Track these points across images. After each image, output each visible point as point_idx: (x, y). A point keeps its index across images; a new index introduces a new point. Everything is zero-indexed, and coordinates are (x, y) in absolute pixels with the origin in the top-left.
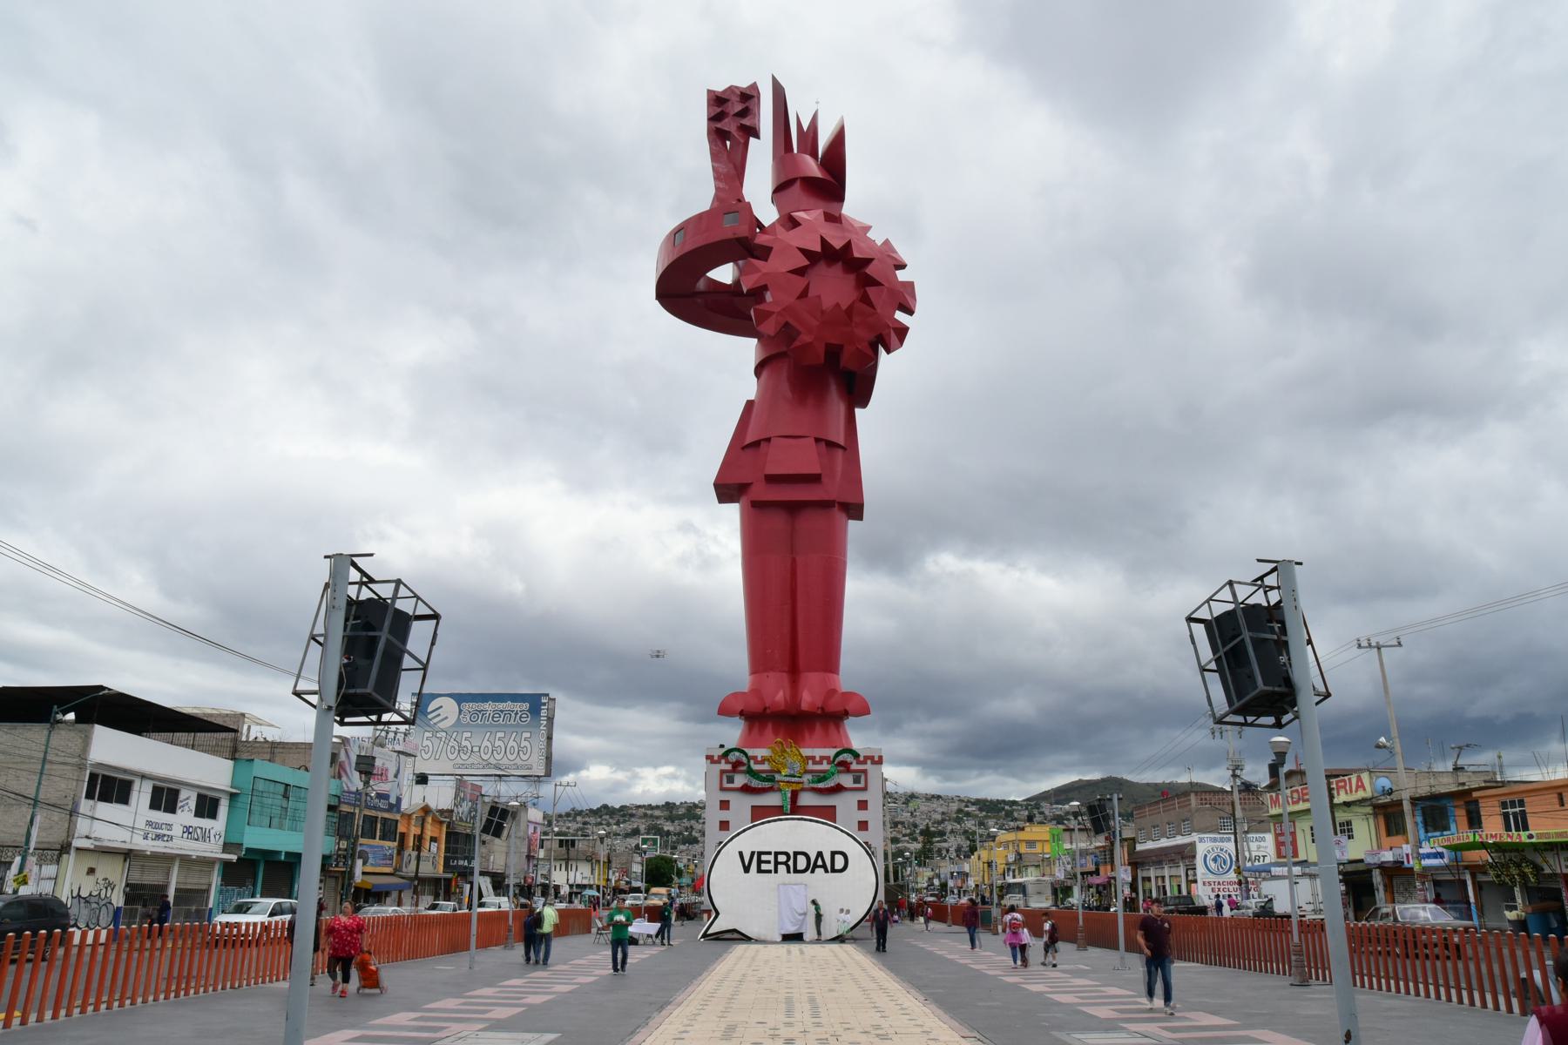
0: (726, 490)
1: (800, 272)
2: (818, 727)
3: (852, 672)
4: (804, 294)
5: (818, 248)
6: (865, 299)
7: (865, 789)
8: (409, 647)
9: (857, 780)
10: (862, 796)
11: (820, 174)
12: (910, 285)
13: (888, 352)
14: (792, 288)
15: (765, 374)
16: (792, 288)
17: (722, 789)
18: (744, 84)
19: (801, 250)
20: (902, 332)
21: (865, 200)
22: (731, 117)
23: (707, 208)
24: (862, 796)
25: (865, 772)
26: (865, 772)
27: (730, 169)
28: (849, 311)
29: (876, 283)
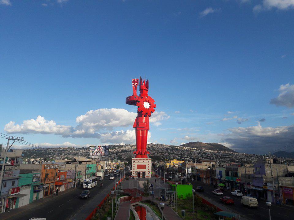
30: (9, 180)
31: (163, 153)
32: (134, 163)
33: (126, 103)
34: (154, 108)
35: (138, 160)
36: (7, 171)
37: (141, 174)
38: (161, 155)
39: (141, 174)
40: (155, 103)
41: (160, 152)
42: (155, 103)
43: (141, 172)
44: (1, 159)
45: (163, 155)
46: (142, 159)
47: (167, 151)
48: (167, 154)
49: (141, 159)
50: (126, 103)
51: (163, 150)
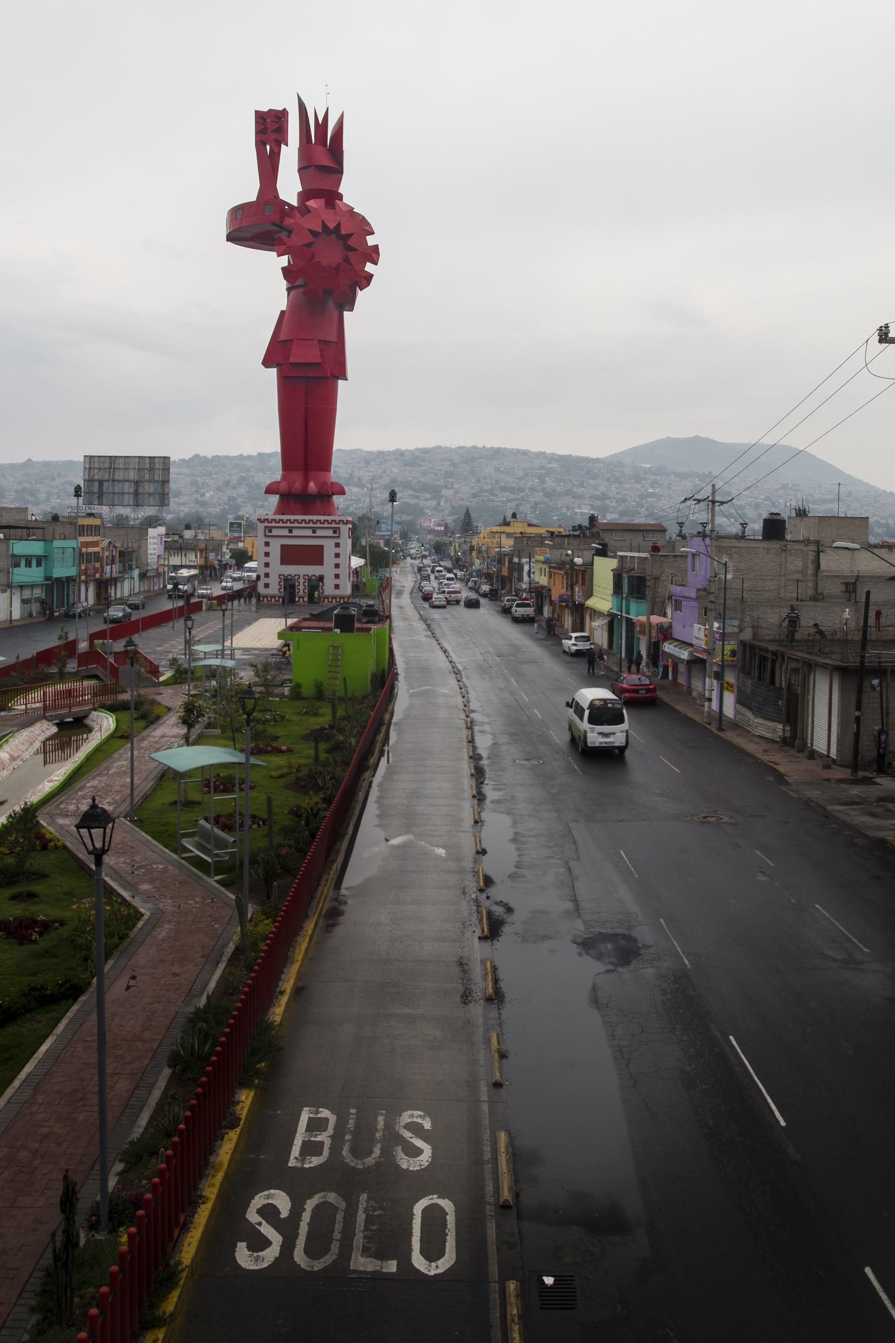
0: (267, 362)
1: (314, 233)
2: (318, 502)
3: (338, 471)
4: (309, 245)
5: (319, 229)
6: (347, 260)
7: (339, 537)
8: (284, 627)
9: (335, 532)
10: (337, 541)
11: (325, 153)
12: (376, 247)
13: (375, 263)
14: (312, 235)
15: (293, 292)
16: (312, 235)
17: (266, 536)
18: (280, 108)
19: (310, 231)
20: (369, 278)
21: (354, 191)
22: (270, 127)
23: (254, 199)
24: (337, 541)
25: (339, 528)
26: (339, 528)
27: (268, 167)
28: (337, 268)
29: (354, 250)
30: (659, 531)
31: (521, 490)
32: (267, 540)
33: (230, 238)
34: (369, 267)
35: (288, 525)
36: (361, 1217)
37: (301, 587)
38: (511, 501)
39: (301, 587)
40: (371, 241)
41: (503, 489)
42: (371, 241)
43: (302, 580)
44: (2, 849)
45: (516, 499)
46: (307, 518)
47: (543, 482)
48: (538, 496)
49: (300, 518)
50: (230, 238)
51: (521, 479)
